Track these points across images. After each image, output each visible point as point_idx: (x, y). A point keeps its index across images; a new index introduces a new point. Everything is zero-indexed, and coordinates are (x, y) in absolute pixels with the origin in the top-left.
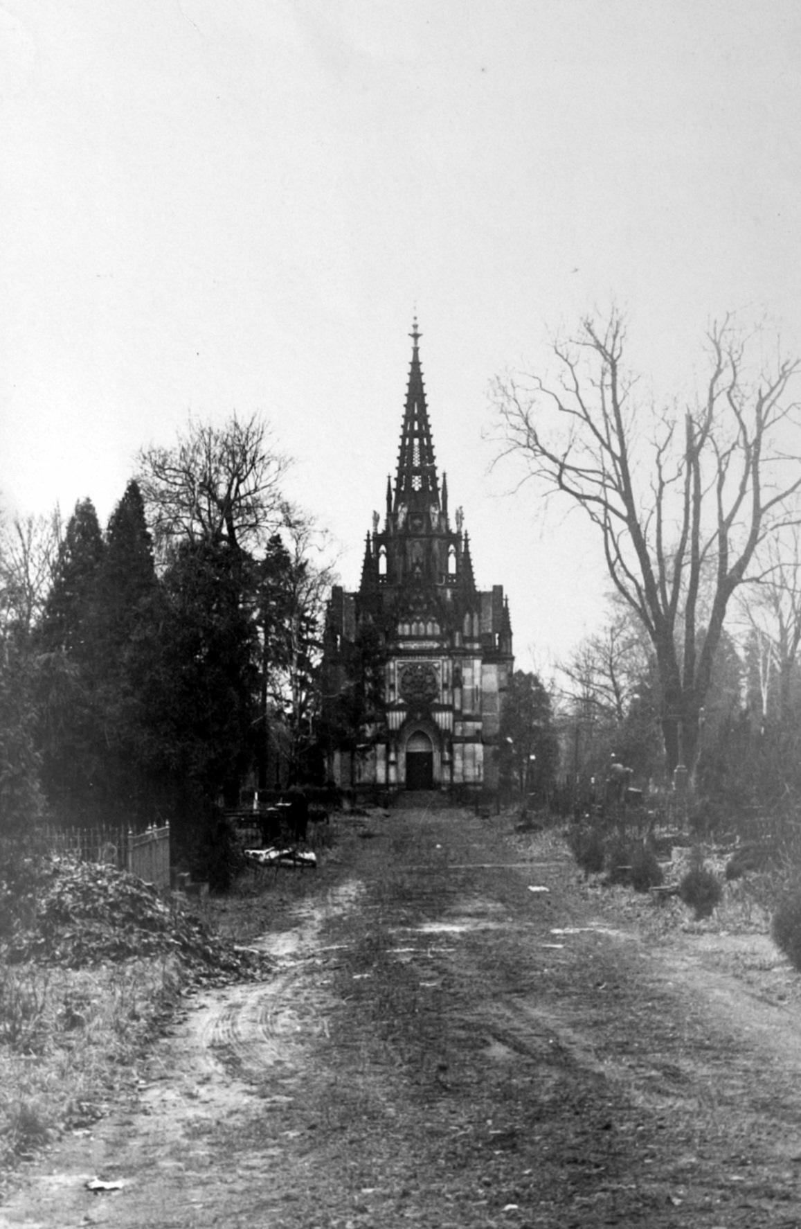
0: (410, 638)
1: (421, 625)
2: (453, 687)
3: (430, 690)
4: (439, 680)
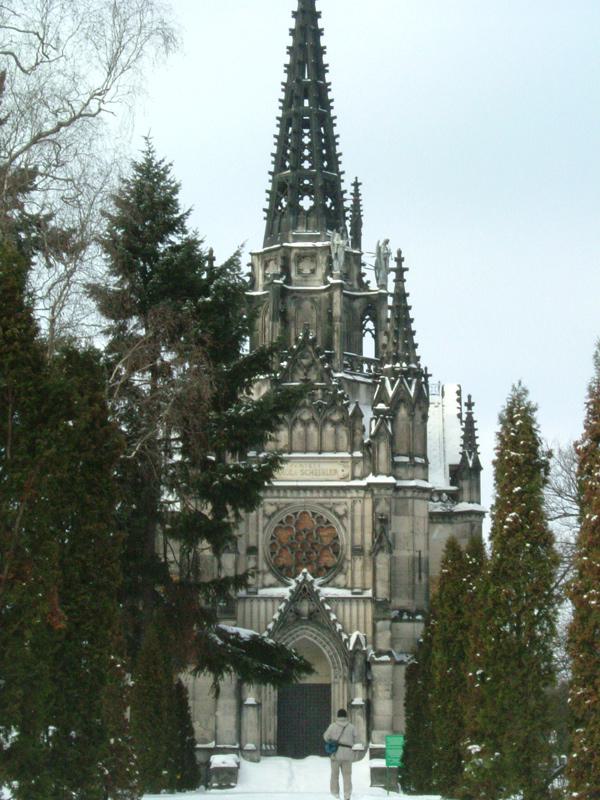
1: (312, 429)
2: (375, 552)
4: (345, 540)
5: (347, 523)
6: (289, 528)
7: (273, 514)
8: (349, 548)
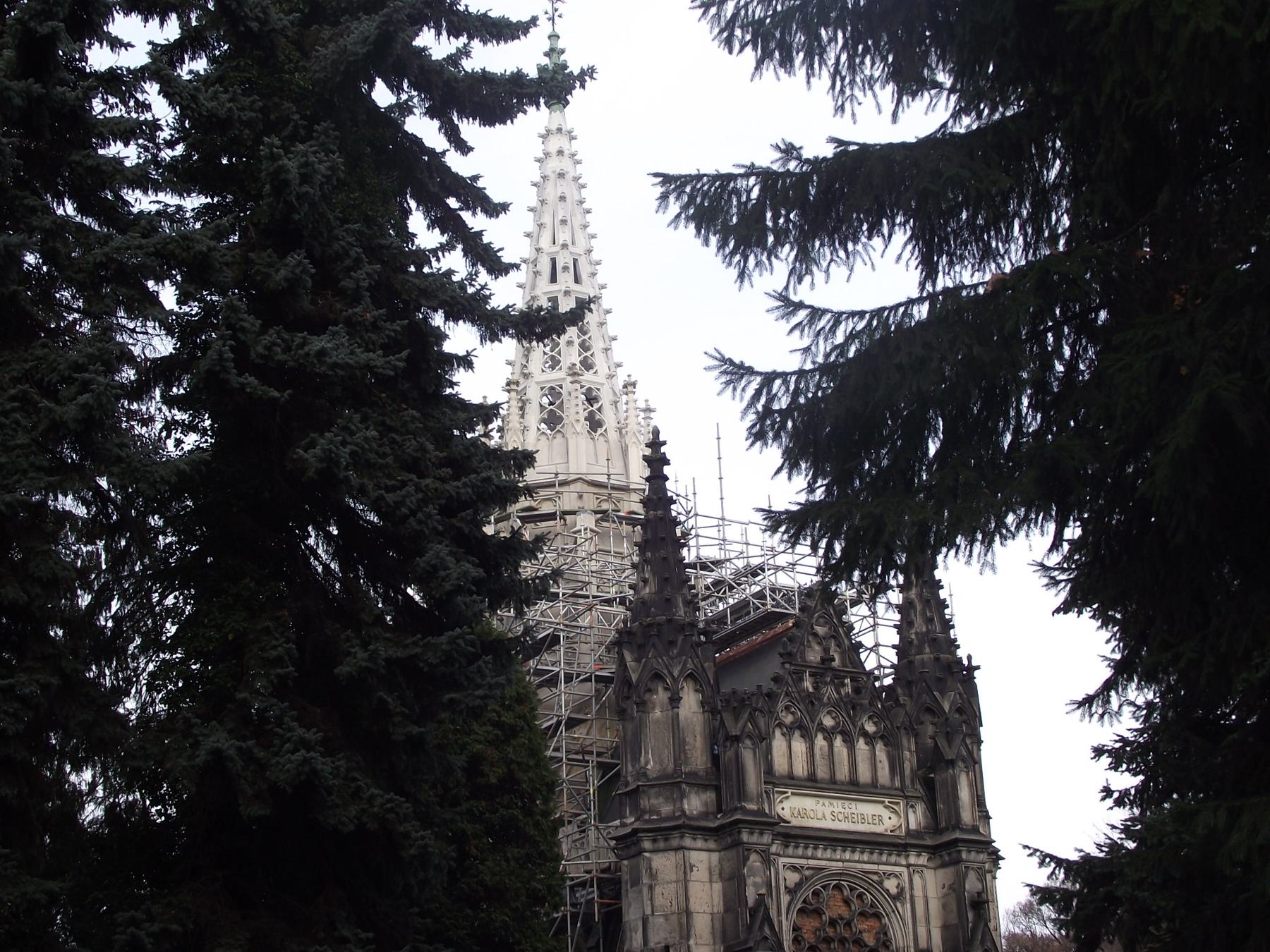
0: (811, 784)
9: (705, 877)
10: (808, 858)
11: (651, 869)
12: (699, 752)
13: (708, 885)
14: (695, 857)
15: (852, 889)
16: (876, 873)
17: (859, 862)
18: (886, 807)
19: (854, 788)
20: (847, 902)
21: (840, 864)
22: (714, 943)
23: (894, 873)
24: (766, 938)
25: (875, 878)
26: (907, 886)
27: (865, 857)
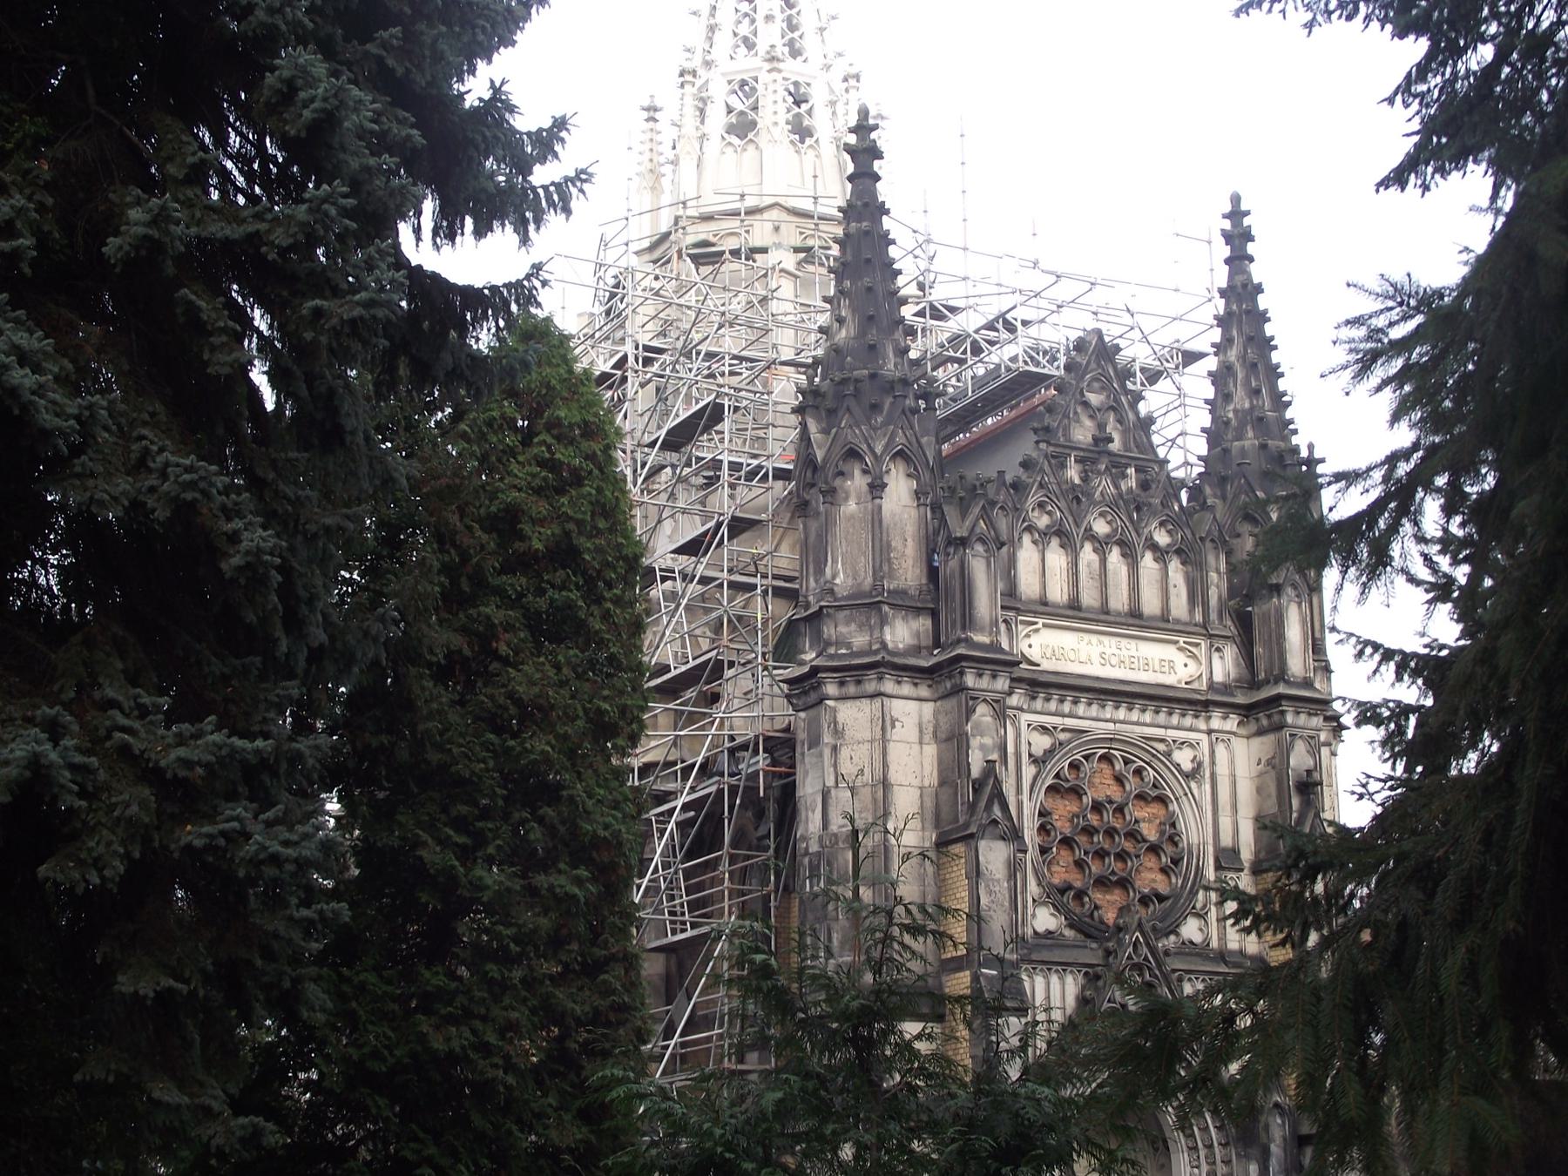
0: (1073, 613)
3: (1150, 878)
5: (1203, 791)
6: (1077, 792)
7: (1050, 753)
8: (1211, 849)
9: (913, 735)
10: (1064, 716)
11: (836, 723)
12: (910, 562)
13: (916, 747)
14: (898, 708)
15: (1127, 762)
16: (1162, 741)
17: (1136, 723)
18: (1181, 649)
19: (1135, 621)
20: (1119, 780)
21: (1111, 726)
22: (923, 829)
23: (1188, 741)
24: (995, 822)
25: (1161, 747)
26: (1207, 761)
27: (1148, 717)
